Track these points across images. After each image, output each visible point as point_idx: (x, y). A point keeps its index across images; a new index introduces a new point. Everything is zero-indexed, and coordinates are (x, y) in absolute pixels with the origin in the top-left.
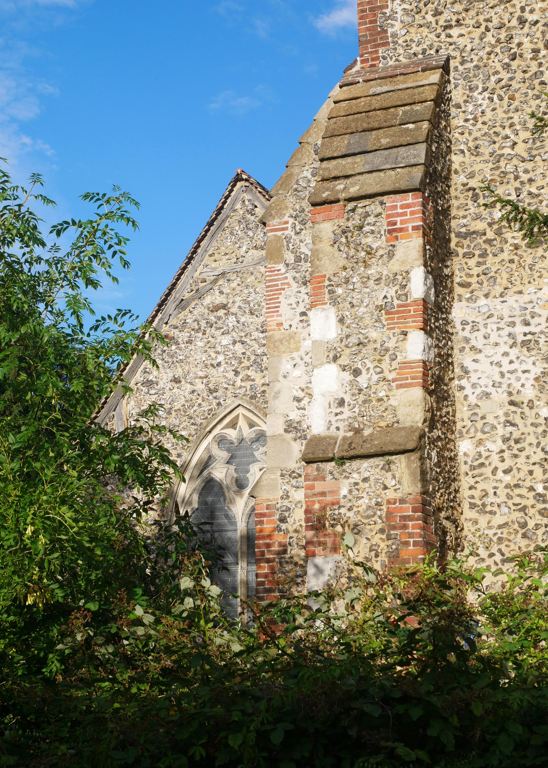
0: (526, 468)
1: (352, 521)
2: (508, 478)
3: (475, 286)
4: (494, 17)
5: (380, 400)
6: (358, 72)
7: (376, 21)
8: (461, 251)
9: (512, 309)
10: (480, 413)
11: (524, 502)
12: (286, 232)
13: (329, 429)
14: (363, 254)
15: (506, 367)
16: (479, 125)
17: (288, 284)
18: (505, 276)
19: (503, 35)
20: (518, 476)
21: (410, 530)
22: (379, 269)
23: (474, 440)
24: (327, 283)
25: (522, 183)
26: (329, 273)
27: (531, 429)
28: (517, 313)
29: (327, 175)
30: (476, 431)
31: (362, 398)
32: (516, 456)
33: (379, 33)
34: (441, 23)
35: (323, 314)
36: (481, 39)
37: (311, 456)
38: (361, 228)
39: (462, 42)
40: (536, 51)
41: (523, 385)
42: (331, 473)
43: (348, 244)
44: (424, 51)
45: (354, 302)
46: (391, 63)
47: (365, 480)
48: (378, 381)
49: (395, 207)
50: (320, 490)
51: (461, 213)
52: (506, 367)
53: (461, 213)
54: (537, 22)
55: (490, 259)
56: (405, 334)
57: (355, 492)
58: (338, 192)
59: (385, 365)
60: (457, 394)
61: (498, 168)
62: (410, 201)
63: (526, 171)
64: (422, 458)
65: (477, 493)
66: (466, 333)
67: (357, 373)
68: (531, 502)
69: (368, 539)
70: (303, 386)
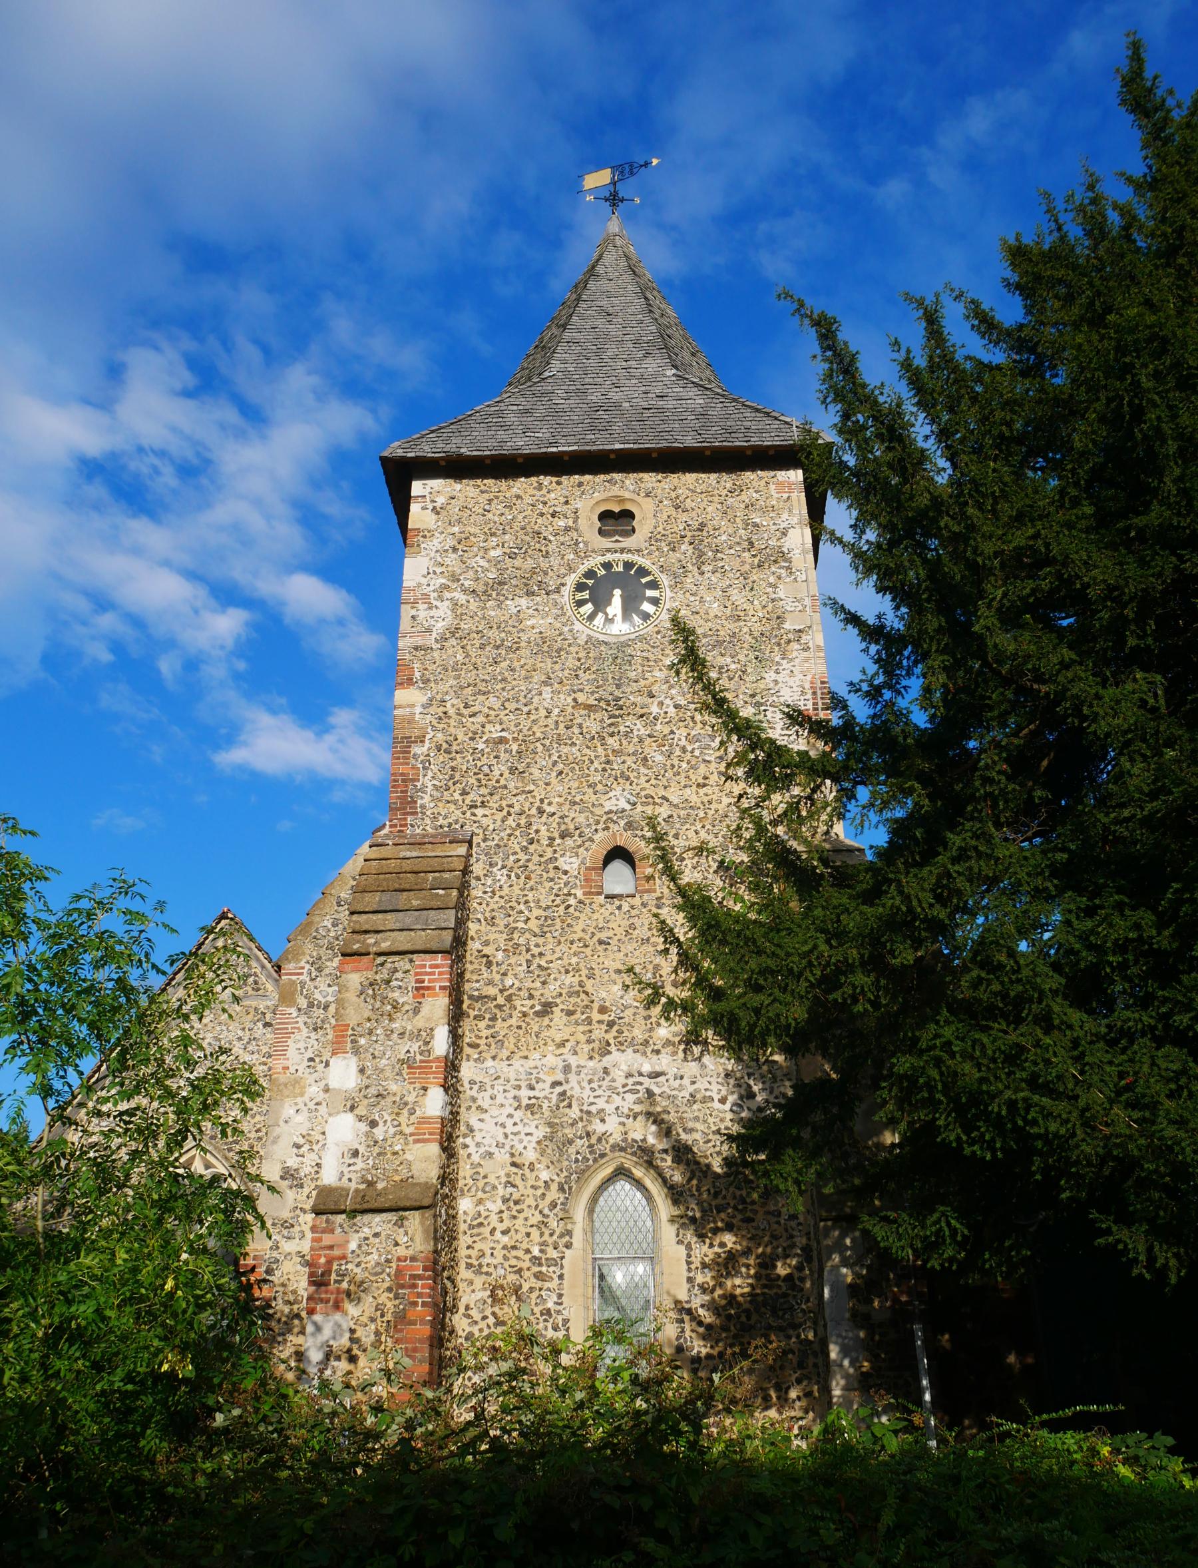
0: (523, 1230)
1: (359, 1278)
2: (505, 1240)
3: (483, 1047)
4: (516, 804)
5: (395, 1153)
6: (386, 835)
7: (406, 792)
8: (472, 1013)
9: (518, 1073)
10: (482, 1172)
11: (520, 1264)
12: (301, 977)
13: (340, 1179)
14: (389, 1007)
15: (510, 1129)
16: (497, 898)
17: (298, 1028)
18: (512, 1040)
19: (523, 822)
20: (516, 1237)
21: (419, 1290)
22: (403, 1024)
23: (475, 1199)
24: (350, 1032)
25: (533, 956)
26: (353, 1023)
27: (531, 1191)
28: (523, 1077)
29: (357, 927)
30: (477, 1190)
31: (376, 1150)
32: (514, 1217)
33: (409, 803)
34: (467, 802)
35: (344, 1062)
36: (503, 822)
37: (322, 1207)
38: (388, 982)
39: (485, 821)
40: (552, 839)
41: (525, 1148)
42: (341, 1226)
43: (374, 997)
44: (450, 825)
45: (376, 1053)
46: (418, 831)
47: (376, 1235)
48: (395, 1134)
49: (424, 966)
50: (329, 1243)
51: (475, 977)
52: (510, 1129)
53: (475, 977)
54: (554, 814)
55: (499, 1023)
56: (425, 1089)
57: (365, 1248)
58: (369, 945)
59: (403, 1119)
60: (461, 1152)
61: (512, 939)
62: (439, 962)
63: (537, 945)
64: (435, 1216)
65: (474, 1253)
66: (474, 1093)
67: (373, 1124)
68: (527, 1264)
69: (374, 1297)
70: (304, 1133)
